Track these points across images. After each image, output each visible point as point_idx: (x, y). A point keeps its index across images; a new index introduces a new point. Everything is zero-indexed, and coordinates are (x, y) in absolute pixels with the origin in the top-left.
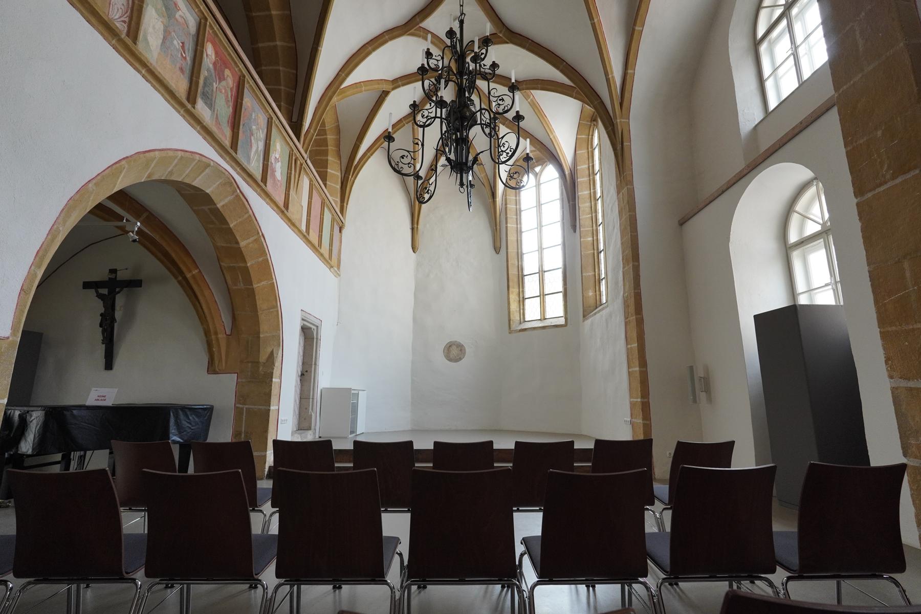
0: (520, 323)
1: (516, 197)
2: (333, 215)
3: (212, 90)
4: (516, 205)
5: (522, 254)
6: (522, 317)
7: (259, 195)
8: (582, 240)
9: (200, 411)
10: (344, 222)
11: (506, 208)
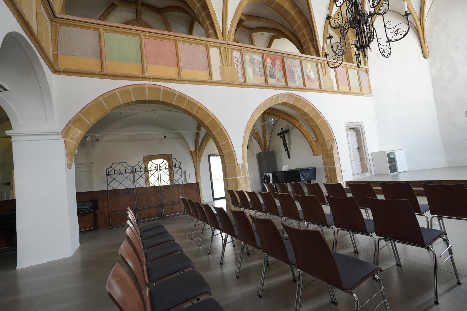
3: (273, 72)
7: (304, 91)
9: (309, 170)
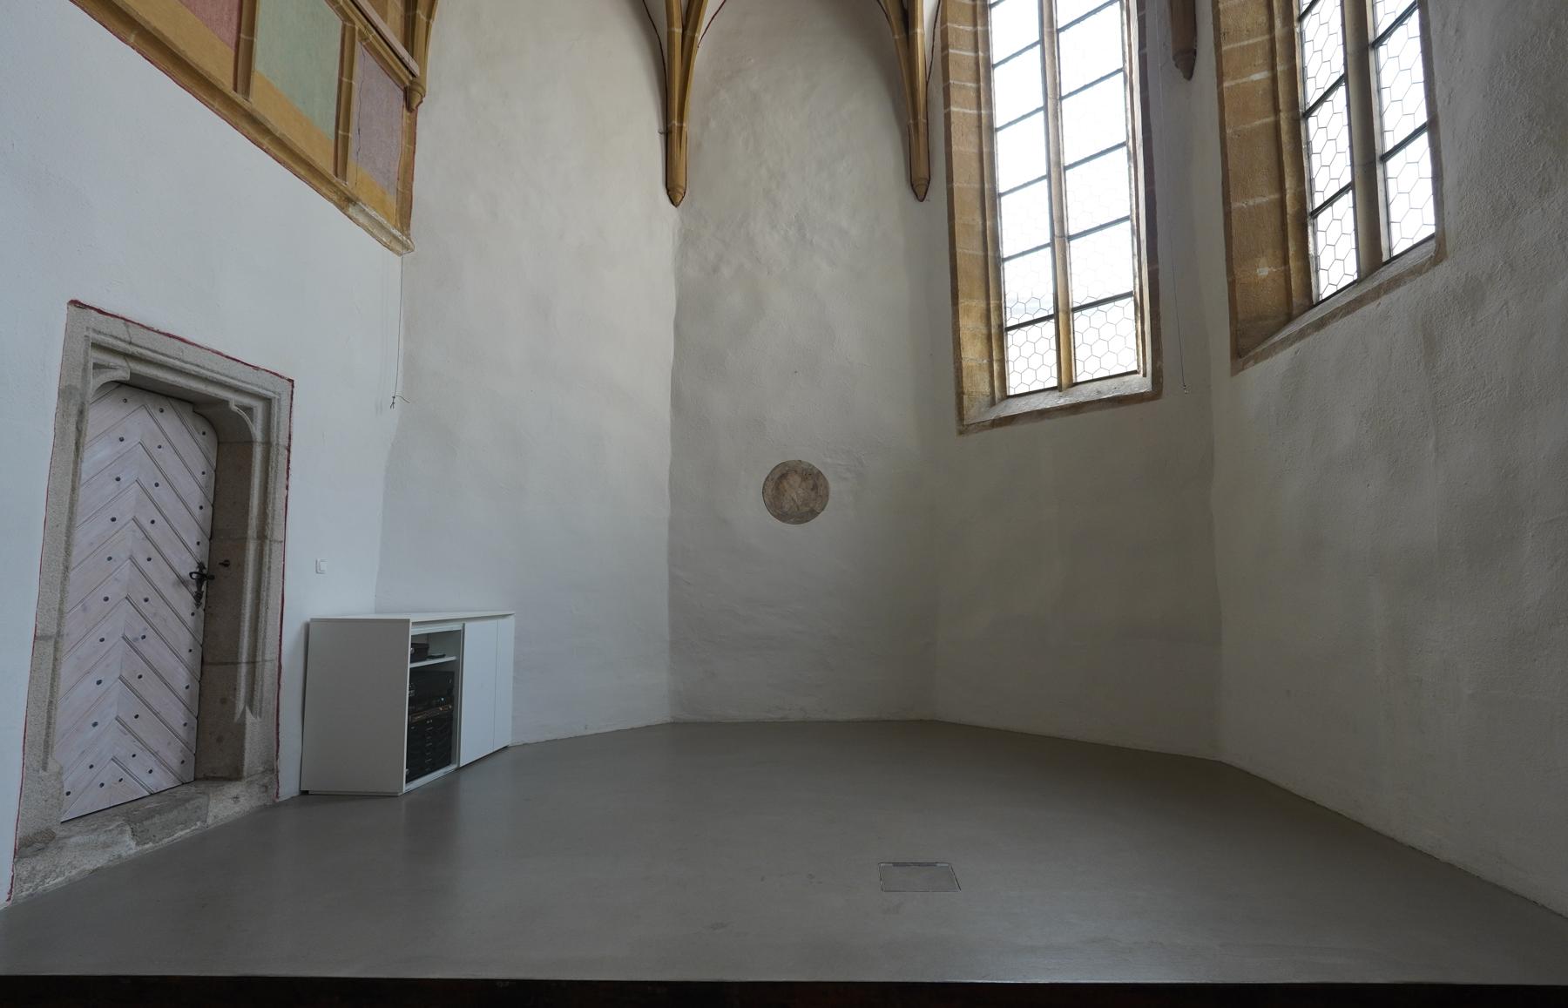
0: (993, 403)
1: (975, 25)
2: (346, 18)
4: (976, 50)
5: (996, 196)
6: (996, 383)
8: (1226, 85)
10: (416, 69)
11: (945, 60)
